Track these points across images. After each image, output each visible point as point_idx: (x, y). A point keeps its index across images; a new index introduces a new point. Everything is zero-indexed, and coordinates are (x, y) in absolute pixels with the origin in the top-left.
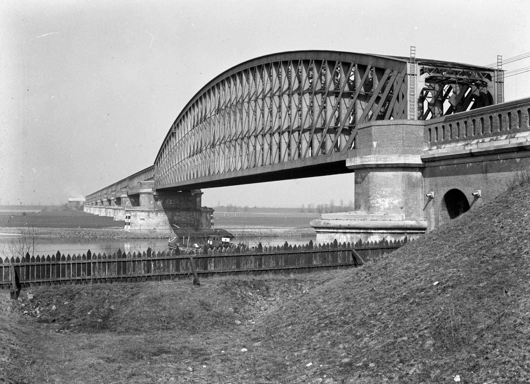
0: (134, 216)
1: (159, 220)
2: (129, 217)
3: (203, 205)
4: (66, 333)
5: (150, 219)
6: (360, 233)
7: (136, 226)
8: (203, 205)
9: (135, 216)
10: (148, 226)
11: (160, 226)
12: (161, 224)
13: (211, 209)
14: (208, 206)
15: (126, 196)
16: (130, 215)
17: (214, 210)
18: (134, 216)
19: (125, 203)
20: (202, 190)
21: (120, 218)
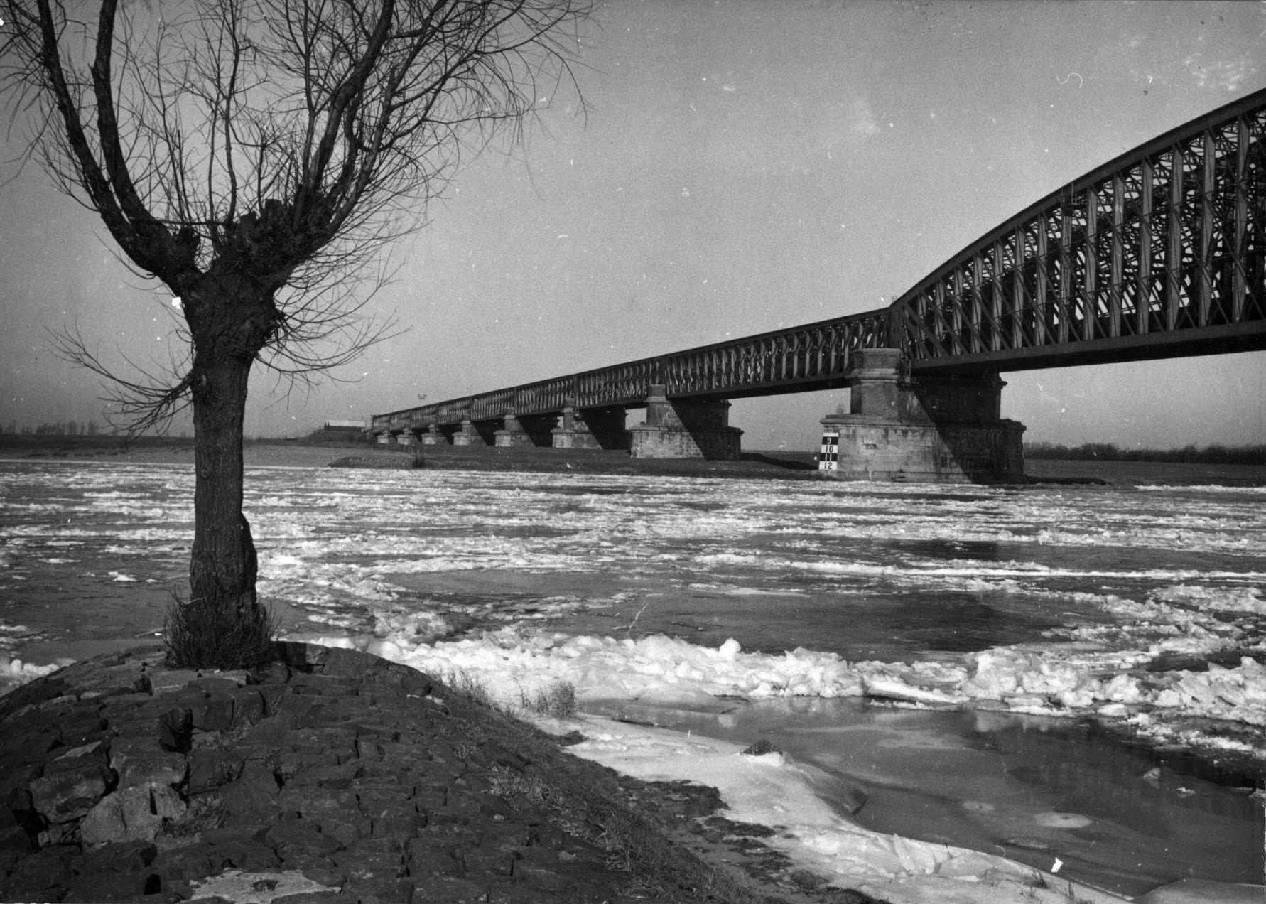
0: (848, 436)
1: (911, 448)
2: (835, 441)
3: (1003, 416)
4: (485, 731)
5: (890, 447)
6: (621, 491)
7: (857, 463)
8: (1003, 416)
9: (852, 437)
10: (886, 463)
11: (915, 464)
12: (915, 458)
13: (1019, 423)
14: (1014, 418)
15: (663, 399)
16: (836, 435)
17: (1025, 428)
18: (848, 436)
19: (660, 416)
20: (730, 401)
21: (649, 453)
